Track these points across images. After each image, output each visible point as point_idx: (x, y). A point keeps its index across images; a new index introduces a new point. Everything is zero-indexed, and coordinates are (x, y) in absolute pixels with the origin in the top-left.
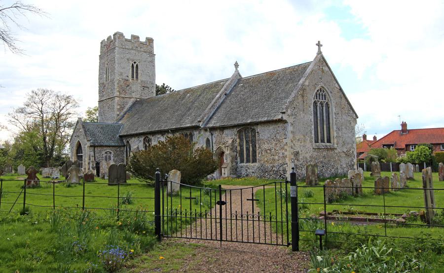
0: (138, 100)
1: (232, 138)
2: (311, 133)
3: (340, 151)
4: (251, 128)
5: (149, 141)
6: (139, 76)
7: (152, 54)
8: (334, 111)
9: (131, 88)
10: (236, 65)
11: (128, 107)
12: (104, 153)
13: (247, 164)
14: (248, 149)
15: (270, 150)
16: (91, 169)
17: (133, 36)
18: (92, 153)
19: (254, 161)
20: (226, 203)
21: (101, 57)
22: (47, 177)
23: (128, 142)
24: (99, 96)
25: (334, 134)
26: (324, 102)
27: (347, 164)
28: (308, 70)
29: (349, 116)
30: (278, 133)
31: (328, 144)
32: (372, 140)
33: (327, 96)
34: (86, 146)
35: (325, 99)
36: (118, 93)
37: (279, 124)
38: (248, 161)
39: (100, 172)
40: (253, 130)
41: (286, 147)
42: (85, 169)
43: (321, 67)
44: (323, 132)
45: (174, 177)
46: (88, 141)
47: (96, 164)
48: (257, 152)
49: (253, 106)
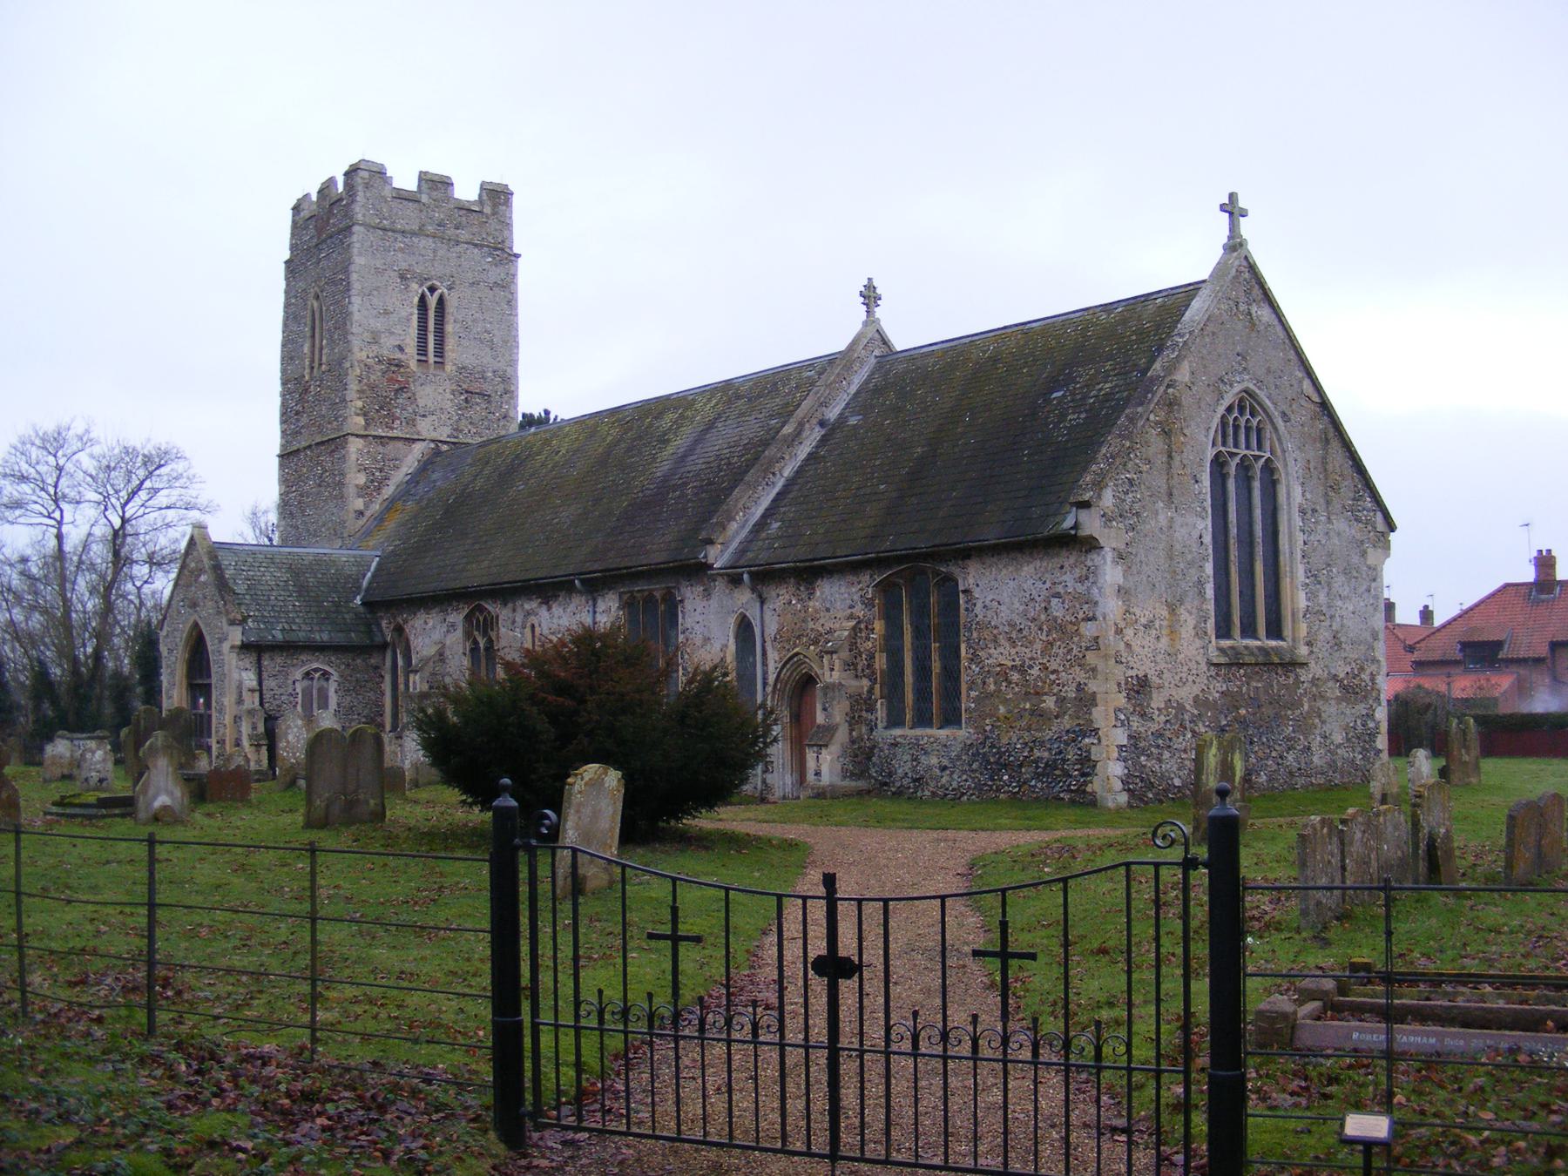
0: (445, 448)
1: (851, 617)
2: (1201, 594)
3: (1319, 673)
4: (938, 573)
5: (489, 624)
6: (450, 344)
7: (504, 255)
8: (1297, 498)
9: (412, 399)
10: (870, 296)
11: (399, 476)
12: (298, 674)
13: (919, 732)
14: (923, 671)
15: (1022, 670)
16: (246, 743)
17: (427, 180)
18: (250, 679)
19: (951, 718)
20: (859, 968)
21: (293, 268)
22: (64, 777)
23: (399, 630)
24: (283, 432)
25: (1296, 598)
26: (1257, 458)
27: (1346, 728)
28: (1197, 309)
29: (1358, 520)
30: (1057, 595)
31: (1273, 643)
32: (1416, 621)
33: (1268, 432)
34: (226, 646)
35: (1260, 448)
36: (361, 421)
37: (1064, 553)
38: (923, 720)
39: (279, 763)
40: (949, 582)
41: (1091, 658)
42: (221, 742)
43: (1243, 307)
44: (1248, 590)
45: (595, 797)
46: (232, 623)
47: (266, 720)
48: (964, 678)
49: (982, 451)
